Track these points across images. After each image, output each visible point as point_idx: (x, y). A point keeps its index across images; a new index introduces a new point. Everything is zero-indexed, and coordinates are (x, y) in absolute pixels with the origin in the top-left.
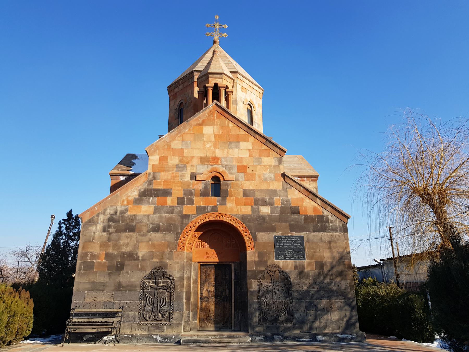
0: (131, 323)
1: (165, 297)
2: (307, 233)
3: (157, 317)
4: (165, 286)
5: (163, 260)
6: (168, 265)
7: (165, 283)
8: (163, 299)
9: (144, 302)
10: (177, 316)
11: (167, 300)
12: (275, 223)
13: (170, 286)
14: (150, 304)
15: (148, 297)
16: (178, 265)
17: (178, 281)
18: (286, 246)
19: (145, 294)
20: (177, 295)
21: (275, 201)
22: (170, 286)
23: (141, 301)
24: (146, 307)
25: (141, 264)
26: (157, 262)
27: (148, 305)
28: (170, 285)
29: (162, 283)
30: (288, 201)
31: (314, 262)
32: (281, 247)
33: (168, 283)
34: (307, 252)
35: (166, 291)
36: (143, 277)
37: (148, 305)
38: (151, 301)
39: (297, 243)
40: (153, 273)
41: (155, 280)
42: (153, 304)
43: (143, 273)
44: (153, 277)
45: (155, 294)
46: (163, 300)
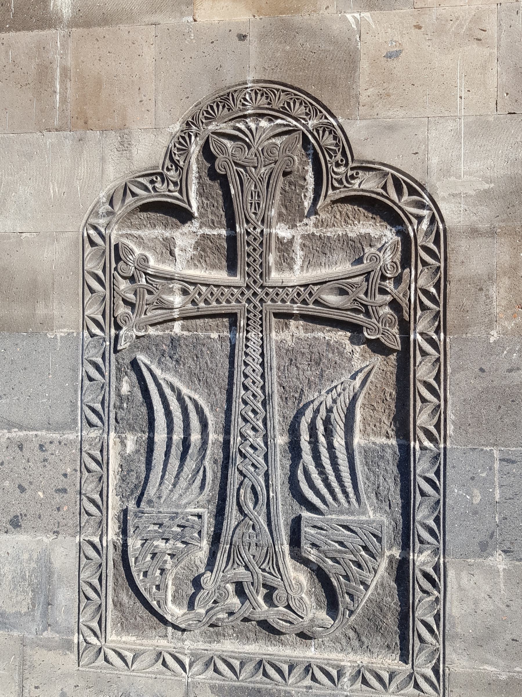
0: (15, 633)
1: (344, 401)
3: (269, 599)
4: (342, 292)
5: (298, 10)
6: (364, 65)
7: (336, 256)
8: (327, 422)
9: (131, 446)
10: (486, 606)
11: (364, 432)
13: (389, 285)
14: (190, 464)
15: (167, 391)
16: (486, 52)
17: (492, 233)
19: (134, 364)
20: (323, 639)
22: (389, 285)
23: (94, 433)
24: (151, 491)
25: (70, 62)
26: (242, 37)
27: (170, 477)
28: (398, 280)
29: (299, 254)
33: (375, 258)
35: (352, 341)
36: (103, 196)
37: (170, 477)
38: (195, 437)
40: (206, 151)
41: (231, 225)
42: (225, 468)
43: (103, 159)
44: (201, 194)
45: (239, 367)
46: (329, 433)
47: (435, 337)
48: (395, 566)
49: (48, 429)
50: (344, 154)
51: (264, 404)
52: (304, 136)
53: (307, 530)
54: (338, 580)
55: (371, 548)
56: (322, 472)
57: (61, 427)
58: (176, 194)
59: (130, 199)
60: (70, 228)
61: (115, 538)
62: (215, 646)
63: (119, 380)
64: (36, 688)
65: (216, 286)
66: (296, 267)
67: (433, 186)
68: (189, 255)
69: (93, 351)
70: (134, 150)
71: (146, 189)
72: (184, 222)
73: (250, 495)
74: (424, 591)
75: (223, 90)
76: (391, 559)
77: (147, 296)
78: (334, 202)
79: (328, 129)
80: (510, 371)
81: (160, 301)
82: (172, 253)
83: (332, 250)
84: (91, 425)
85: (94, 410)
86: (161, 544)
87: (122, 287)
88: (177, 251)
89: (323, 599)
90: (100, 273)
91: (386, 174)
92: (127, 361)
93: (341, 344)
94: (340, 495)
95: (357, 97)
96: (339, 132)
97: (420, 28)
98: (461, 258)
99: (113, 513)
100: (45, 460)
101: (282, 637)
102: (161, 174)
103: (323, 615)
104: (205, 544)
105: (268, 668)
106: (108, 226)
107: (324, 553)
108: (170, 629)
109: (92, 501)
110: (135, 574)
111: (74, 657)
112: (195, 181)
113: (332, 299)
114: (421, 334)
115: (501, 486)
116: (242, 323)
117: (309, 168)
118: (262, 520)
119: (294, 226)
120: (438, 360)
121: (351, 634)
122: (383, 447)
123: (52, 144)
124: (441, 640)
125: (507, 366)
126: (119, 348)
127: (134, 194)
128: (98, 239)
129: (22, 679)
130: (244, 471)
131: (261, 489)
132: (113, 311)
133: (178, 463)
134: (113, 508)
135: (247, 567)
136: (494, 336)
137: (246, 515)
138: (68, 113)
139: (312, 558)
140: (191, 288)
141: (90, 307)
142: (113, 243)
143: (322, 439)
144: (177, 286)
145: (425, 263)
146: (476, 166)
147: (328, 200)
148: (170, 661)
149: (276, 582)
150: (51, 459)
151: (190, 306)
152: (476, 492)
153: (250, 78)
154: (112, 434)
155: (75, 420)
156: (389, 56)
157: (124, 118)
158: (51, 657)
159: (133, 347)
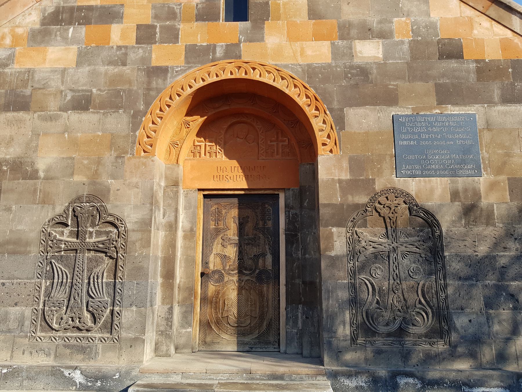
0: (13, 334)
2: (483, 107)
4: (103, 244)
5: (97, 179)
6: (112, 192)
8: (97, 276)
9: (48, 284)
12: (394, 83)
14: (63, 287)
15: (58, 269)
16: (139, 190)
17: (137, 231)
18: (425, 140)
19: (51, 263)
21: (394, 26)
22: (114, 243)
23: (39, 280)
24: (52, 295)
25: (42, 188)
26: (84, 184)
29: (94, 235)
30: (432, 26)
31: (507, 182)
32: (412, 143)
34: (486, 155)
38: (65, 281)
39: (458, 133)
40: (74, 211)
41: (78, 228)
43: (48, 212)
44: (72, 220)
47: (124, 255)
48: (111, 311)
49: (27, 279)
50: (106, 212)
51: (82, 272)
52: (97, 207)
53: (90, 303)
54: (97, 315)
55: (105, 307)
56: (95, 289)
57: (30, 279)
58: (65, 220)
59: (54, 221)
60: (38, 228)
61: (42, 308)
62: (65, 334)
63: (47, 266)
64: (17, 349)
65: (73, 243)
66: (93, 238)
67: (125, 220)
68: (67, 235)
69: (41, 259)
70: (56, 209)
71: (58, 219)
72: (67, 227)
73: (395, 275)
74: (117, 317)
75: (78, 196)
76: (110, 309)
77: (56, 245)
78: (103, 223)
79: (102, 206)
80: (139, 262)
81: (59, 246)
82: (63, 234)
83: (102, 234)
84: (38, 278)
85: (39, 274)
86: (53, 308)
87: (50, 243)
88: (64, 234)
89: (93, 321)
90: (44, 239)
91: (115, 217)
92: (49, 262)
93: (103, 257)
94: (99, 294)
95: (109, 199)
96: (105, 207)
97: (124, 184)
98: (130, 237)
99: (42, 301)
100: (26, 287)
101: (82, 331)
102: (62, 215)
103: (93, 325)
104: (65, 308)
105: (78, 339)
106: (48, 228)
107: (94, 308)
108: (54, 331)
109: (37, 298)
110: (46, 316)
111: (28, 339)
112: (70, 217)
113: (101, 246)
114: (121, 254)
115: (136, 290)
116: (78, 252)
117: (98, 215)
118: (79, 301)
119: (93, 228)
120: (124, 260)
121: (100, 329)
122: (111, 282)
123: (35, 207)
124: (120, 329)
125: (139, 261)
126: (47, 258)
127: (55, 220)
128: (45, 231)
129: (13, 347)
130: (76, 288)
131: (80, 293)
132: (47, 249)
133: (60, 287)
134: (42, 300)
135: (75, 313)
136: (137, 254)
137: (75, 300)
138: (40, 200)
139: (91, 310)
140: (67, 243)
141: (41, 248)
142: (48, 232)
143: (96, 280)
144: (63, 243)
145: (123, 238)
146: (135, 215)
147: (101, 222)
148: (53, 339)
149: (81, 316)
150: (27, 287)
151: (66, 247)
152: (130, 292)
153: (85, 194)
154: (44, 281)
155: (34, 277)
156: (117, 190)
157: (54, 202)
158: (21, 340)
159: (51, 258)
